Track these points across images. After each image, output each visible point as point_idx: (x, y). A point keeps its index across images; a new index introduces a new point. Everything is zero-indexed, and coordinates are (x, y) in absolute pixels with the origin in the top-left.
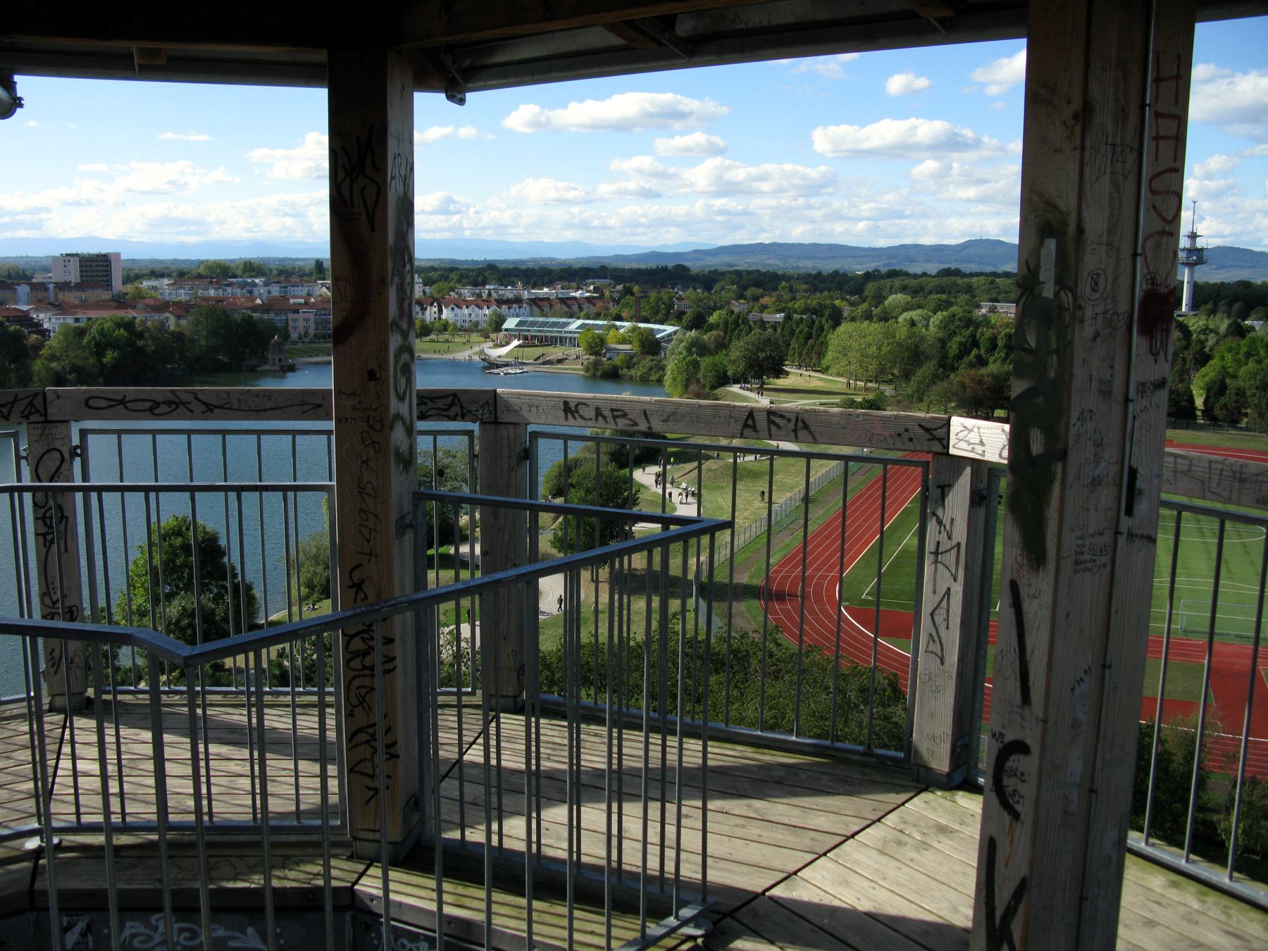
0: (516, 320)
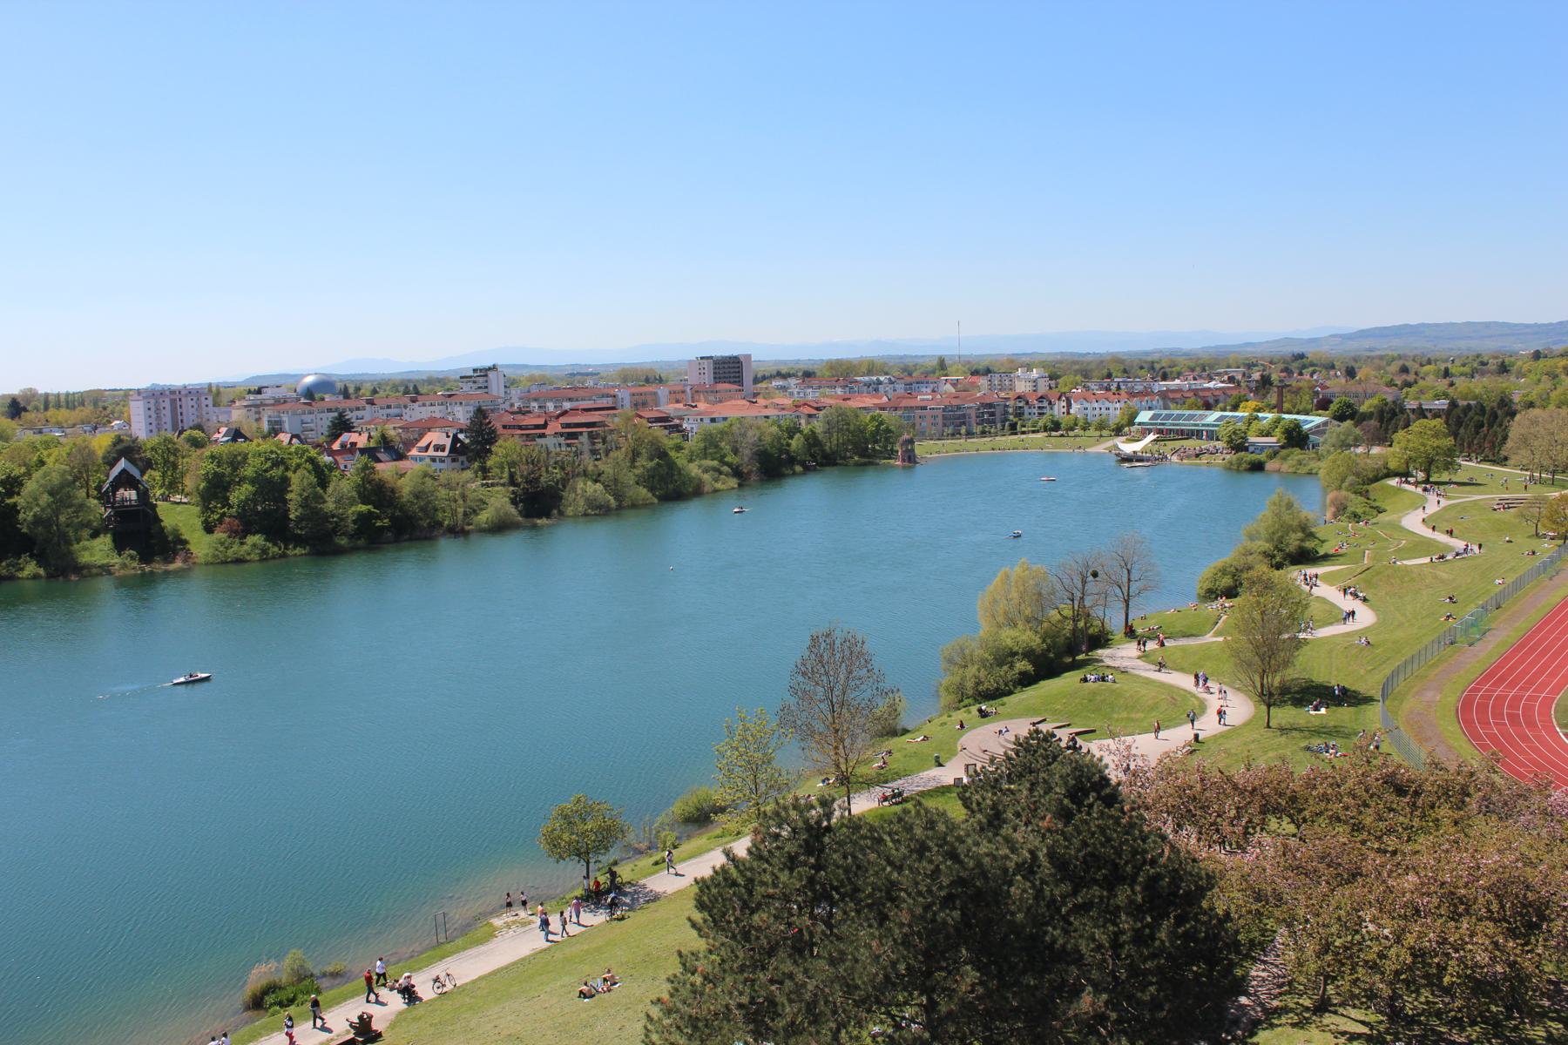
0: (1151, 413)
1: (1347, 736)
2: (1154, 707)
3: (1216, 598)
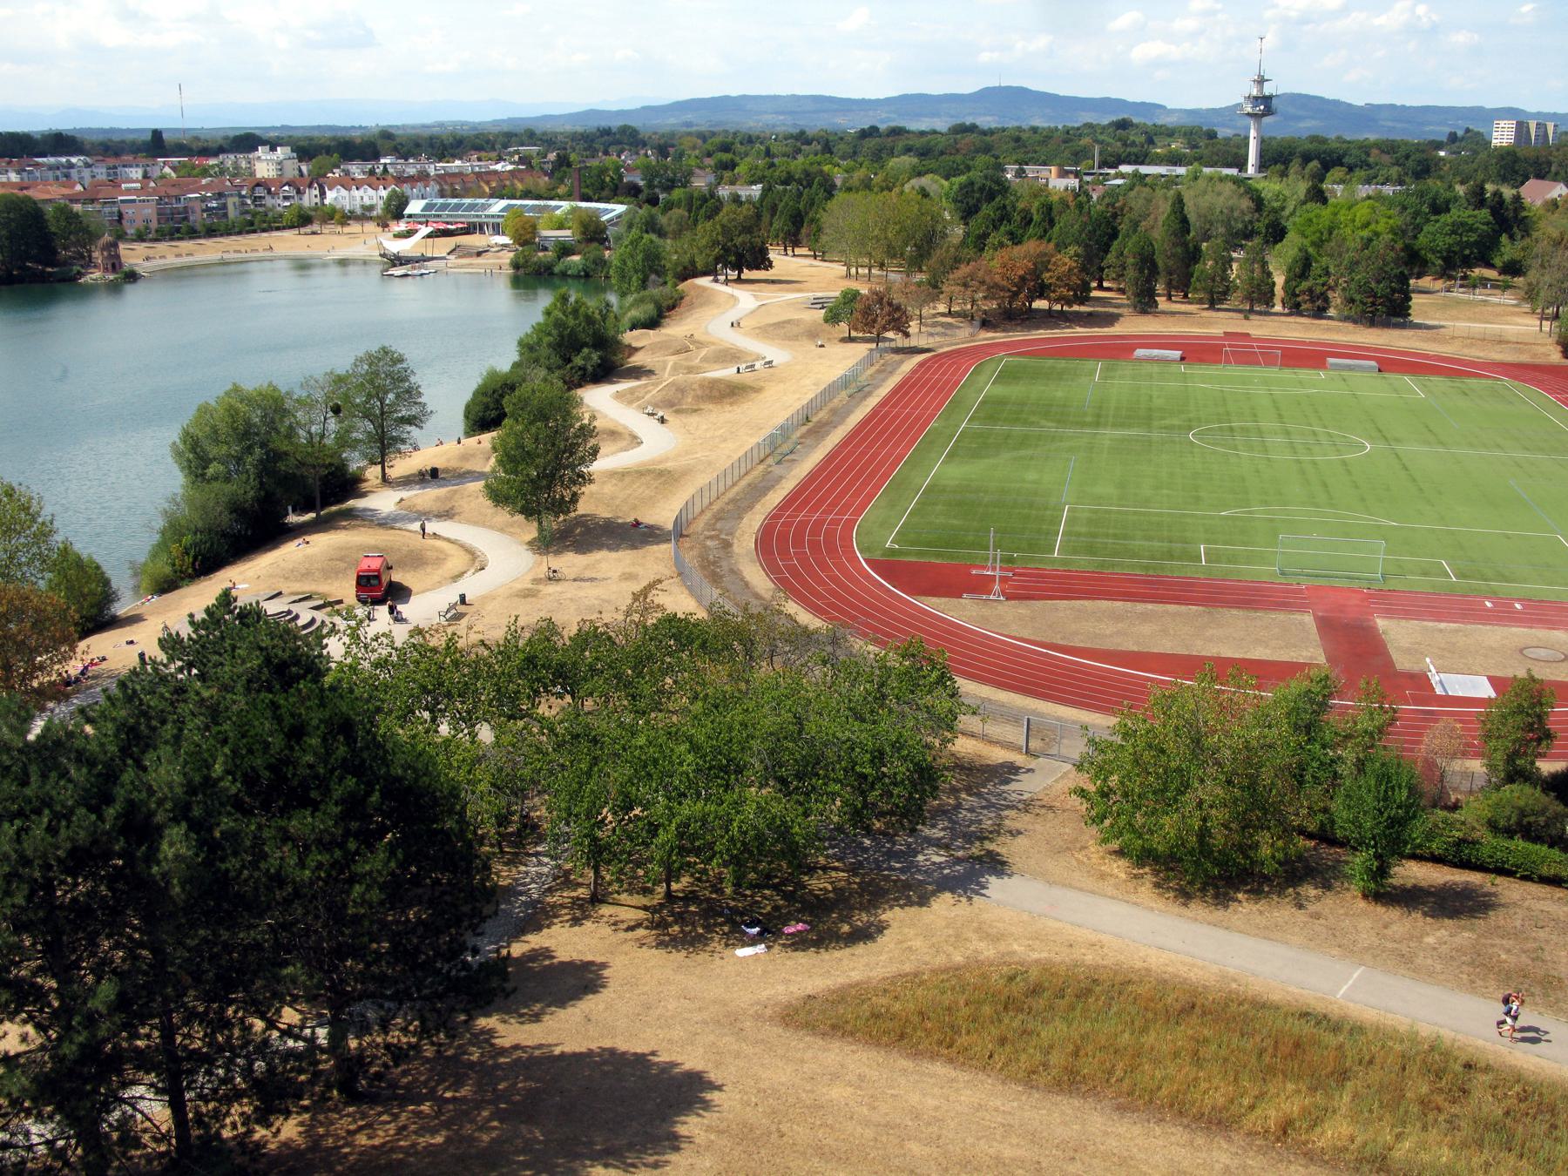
0: (423, 203)
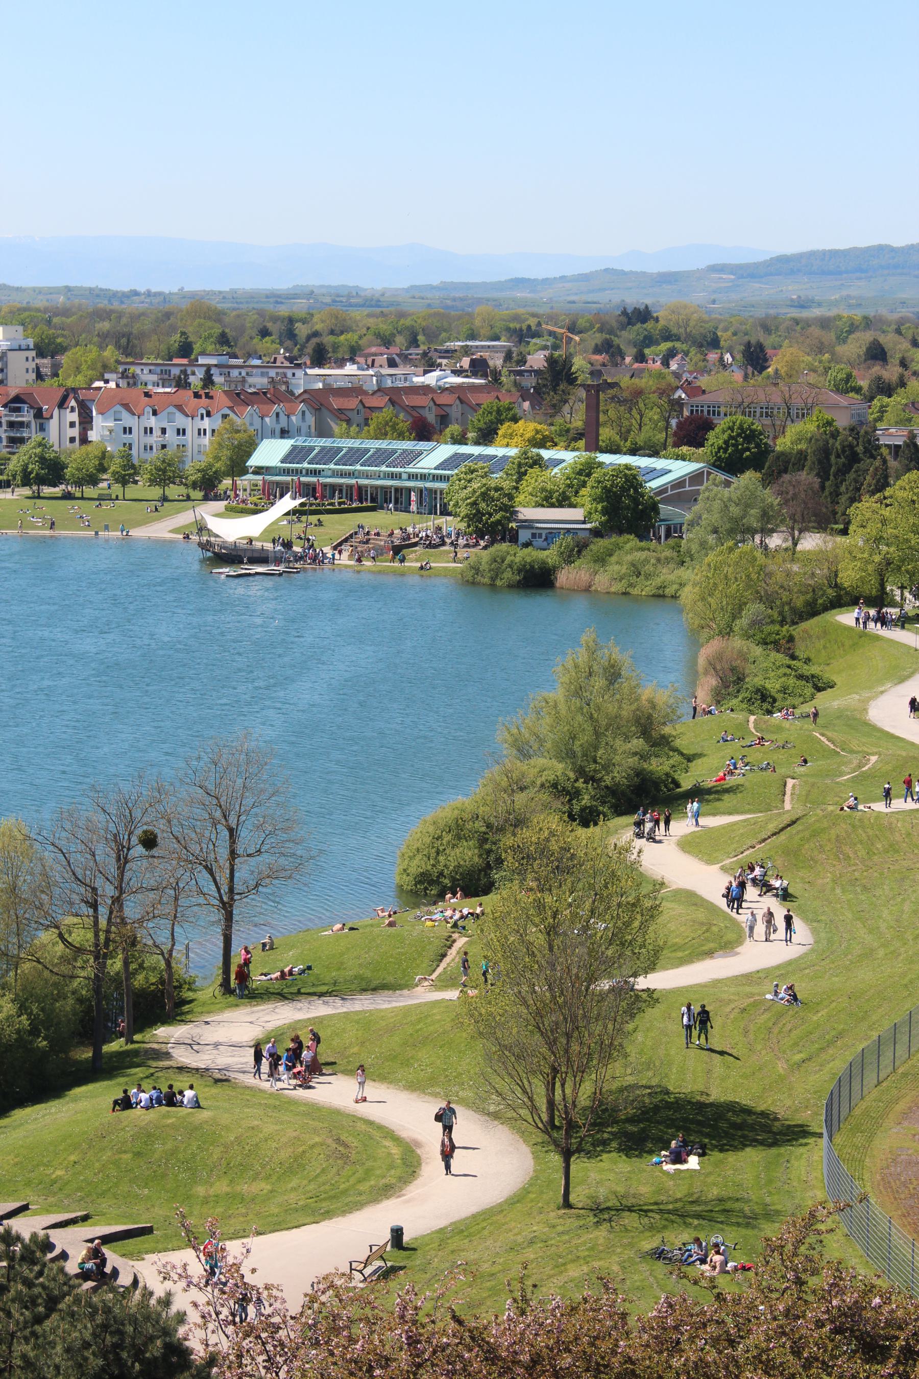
0: (284, 446)
1: (749, 1221)
2: (295, 1166)
3: (441, 896)
